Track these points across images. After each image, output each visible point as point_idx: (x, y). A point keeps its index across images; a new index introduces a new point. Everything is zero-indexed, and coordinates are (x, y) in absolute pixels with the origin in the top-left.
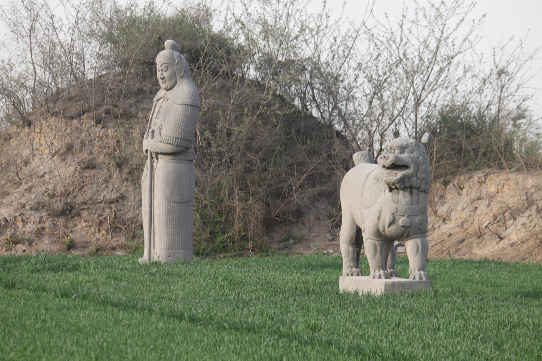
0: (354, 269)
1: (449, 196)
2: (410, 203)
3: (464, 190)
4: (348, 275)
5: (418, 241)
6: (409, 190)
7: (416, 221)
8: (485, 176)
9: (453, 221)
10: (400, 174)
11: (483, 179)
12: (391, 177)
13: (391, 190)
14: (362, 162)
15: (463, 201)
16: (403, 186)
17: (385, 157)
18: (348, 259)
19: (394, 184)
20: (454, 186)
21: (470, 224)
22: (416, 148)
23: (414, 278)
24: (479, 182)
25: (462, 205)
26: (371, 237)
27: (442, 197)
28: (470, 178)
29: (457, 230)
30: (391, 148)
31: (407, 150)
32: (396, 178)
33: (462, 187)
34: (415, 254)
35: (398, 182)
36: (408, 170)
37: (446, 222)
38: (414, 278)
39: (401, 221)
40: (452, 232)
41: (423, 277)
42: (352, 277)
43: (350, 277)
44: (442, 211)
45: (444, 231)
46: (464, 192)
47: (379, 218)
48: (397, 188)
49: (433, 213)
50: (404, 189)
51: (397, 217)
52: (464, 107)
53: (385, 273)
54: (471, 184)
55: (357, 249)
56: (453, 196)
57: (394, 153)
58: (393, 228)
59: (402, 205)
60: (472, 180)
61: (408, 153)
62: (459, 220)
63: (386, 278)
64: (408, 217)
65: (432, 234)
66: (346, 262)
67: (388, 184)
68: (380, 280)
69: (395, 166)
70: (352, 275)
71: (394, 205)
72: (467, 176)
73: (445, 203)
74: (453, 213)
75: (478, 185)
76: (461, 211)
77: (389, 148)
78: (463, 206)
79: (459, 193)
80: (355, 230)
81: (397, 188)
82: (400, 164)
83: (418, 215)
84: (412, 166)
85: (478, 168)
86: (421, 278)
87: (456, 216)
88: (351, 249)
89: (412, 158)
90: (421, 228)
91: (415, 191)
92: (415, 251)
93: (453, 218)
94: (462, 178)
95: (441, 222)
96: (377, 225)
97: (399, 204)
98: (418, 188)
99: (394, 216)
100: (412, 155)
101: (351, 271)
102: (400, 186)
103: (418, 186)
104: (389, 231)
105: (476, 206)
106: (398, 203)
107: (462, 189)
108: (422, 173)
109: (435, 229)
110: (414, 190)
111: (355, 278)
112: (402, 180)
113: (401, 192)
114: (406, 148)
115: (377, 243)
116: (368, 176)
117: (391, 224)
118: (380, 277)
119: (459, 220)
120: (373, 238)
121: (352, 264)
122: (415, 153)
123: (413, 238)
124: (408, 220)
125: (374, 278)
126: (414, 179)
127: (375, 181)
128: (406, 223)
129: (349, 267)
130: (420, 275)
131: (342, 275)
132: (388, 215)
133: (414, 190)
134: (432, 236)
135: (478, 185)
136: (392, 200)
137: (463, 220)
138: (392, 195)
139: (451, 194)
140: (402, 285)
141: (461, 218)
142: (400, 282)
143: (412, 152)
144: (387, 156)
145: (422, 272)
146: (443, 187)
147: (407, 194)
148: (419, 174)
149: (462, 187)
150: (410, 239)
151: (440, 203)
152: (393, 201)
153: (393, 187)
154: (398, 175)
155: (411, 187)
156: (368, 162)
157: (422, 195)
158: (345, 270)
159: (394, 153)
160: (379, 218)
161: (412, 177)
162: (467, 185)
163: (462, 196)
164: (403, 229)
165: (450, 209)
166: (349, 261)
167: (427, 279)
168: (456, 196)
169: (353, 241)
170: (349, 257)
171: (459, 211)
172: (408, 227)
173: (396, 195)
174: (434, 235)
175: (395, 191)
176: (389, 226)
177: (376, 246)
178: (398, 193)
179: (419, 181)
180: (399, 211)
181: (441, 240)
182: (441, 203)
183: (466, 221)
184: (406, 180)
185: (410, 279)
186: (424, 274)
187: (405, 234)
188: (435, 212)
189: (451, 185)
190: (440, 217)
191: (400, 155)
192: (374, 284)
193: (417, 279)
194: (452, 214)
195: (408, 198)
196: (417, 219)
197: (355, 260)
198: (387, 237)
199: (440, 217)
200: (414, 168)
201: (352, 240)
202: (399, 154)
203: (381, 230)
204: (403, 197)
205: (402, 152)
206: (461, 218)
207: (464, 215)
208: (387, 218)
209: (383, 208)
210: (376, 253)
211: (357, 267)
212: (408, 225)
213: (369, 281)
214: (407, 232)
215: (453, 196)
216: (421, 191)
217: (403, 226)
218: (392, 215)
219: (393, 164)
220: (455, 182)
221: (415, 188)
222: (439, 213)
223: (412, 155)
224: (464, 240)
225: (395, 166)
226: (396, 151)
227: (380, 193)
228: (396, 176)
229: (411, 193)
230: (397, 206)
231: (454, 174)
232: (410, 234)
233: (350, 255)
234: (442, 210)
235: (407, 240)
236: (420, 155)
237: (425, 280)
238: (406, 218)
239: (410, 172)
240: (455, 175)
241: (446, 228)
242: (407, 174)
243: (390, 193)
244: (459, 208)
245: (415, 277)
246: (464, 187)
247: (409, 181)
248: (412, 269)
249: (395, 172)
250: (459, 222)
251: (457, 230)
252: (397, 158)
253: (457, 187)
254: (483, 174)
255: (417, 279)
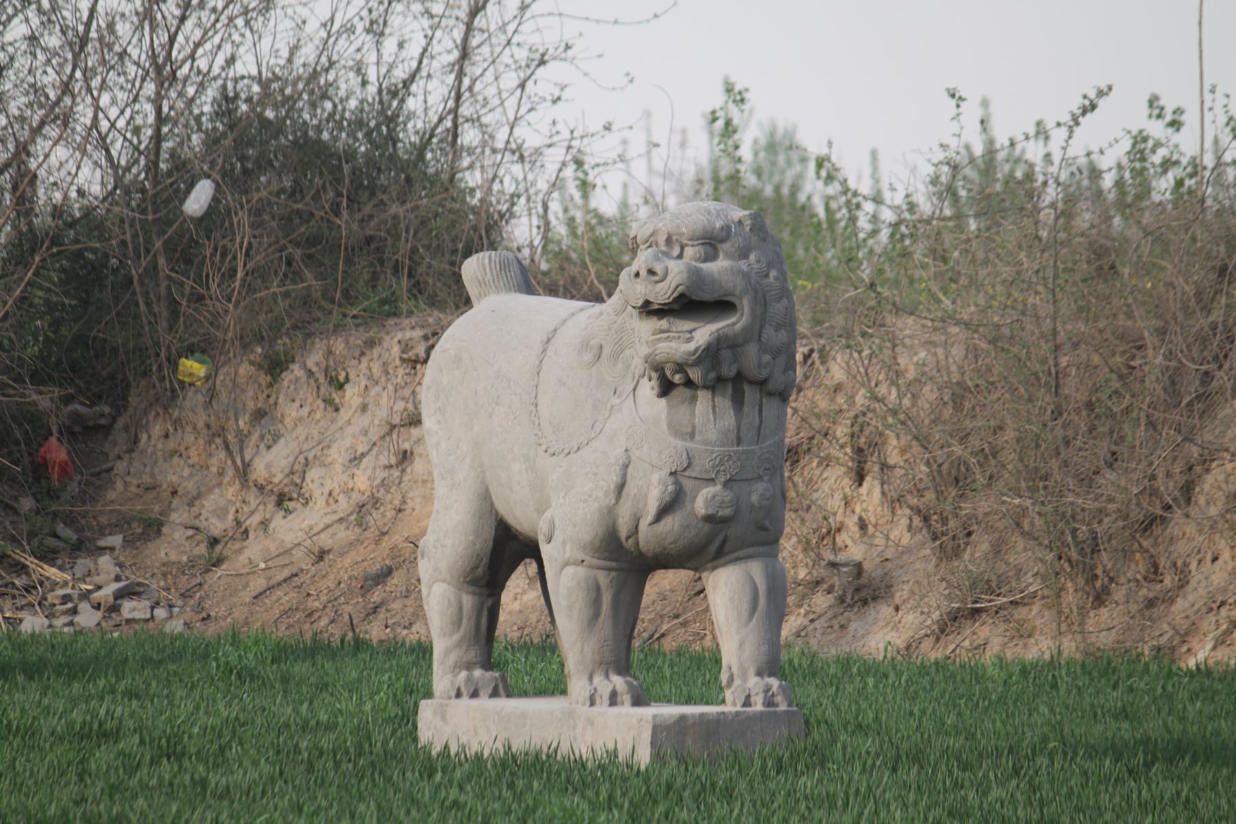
0: (478, 673)
1: (291, 412)
2: (733, 436)
3: (350, 390)
4: (459, 695)
5: (756, 568)
6: (730, 391)
7: (754, 498)
8: (426, 338)
9: (319, 502)
10: (703, 333)
11: (421, 350)
12: (673, 344)
13: (666, 388)
14: (498, 290)
15: (349, 430)
16: (712, 375)
17: (651, 272)
18: (456, 637)
19: (680, 368)
20: (310, 373)
21: (390, 514)
22: (754, 240)
23: (747, 703)
24: (403, 360)
25: (348, 442)
26: (580, 555)
27: (260, 415)
28: (371, 344)
29: (343, 534)
30: (669, 242)
31: (727, 246)
32: (691, 346)
33: (342, 378)
34: (745, 614)
35: (697, 363)
36: (733, 320)
37: (291, 505)
38: (747, 703)
39: (703, 501)
40: (325, 540)
41: (779, 699)
42: (475, 702)
43: (465, 701)
44: (268, 466)
45: (289, 539)
46: (352, 395)
47: (621, 487)
48: (689, 383)
49: (230, 472)
50: (714, 386)
51: (688, 484)
52: (316, 83)
53: (630, 685)
54: (376, 369)
55: (490, 602)
56: (306, 410)
57: (680, 256)
58: (671, 523)
59: (706, 443)
60: (376, 352)
61: (729, 256)
62: (341, 498)
63: (638, 702)
64: (726, 484)
65: (240, 551)
66: (445, 646)
67: (659, 369)
68: (615, 710)
69: (688, 305)
70: (475, 695)
71: (680, 444)
72: (358, 337)
73: (277, 437)
74: (314, 474)
75: (401, 371)
76: (346, 468)
77: (662, 239)
78: (353, 448)
79: (328, 402)
80: (489, 533)
81: (689, 383)
82: (707, 297)
83: (760, 478)
84: (746, 304)
85: (389, 310)
86: (769, 703)
87: (329, 486)
88: (468, 601)
89: (746, 276)
90: (767, 523)
91: (750, 394)
92: (745, 607)
93: (317, 494)
94: (339, 345)
95: (271, 506)
96: (610, 513)
97: (697, 437)
98: (762, 384)
99: (677, 483)
100: (743, 265)
101: (469, 680)
102: (704, 377)
103: (765, 373)
104: (649, 536)
105: (407, 446)
106: (692, 435)
107: (341, 386)
108: (777, 329)
109: (246, 532)
110: (746, 387)
111: (485, 703)
112: (711, 354)
113: (703, 396)
114: (723, 241)
115: (603, 578)
116: (549, 340)
117: (664, 511)
118: (614, 700)
119: (341, 498)
120: (588, 559)
121: (472, 655)
122: (753, 257)
123: (738, 559)
124: (728, 496)
125: (592, 704)
126: (752, 349)
127: (588, 357)
128: (722, 505)
129: (457, 667)
130: (766, 691)
131: (429, 694)
132: (655, 478)
133: (746, 387)
134: (243, 559)
135: (401, 371)
136: (670, 425)
137: (356, 497)
138: (669, 406)
139: (296, 405)
140: (712, 728)
141: (348, 492)
142: (702, 715)
143: (744, 254)
144: (658, 268)
145: (774, 683)
146: (264, 379)
147: (724, 402)
148: (769, 332)
149: (342, 378)
150: (725, 565)
151: (255, 437)
152: (675, 430)
153: (677, 378)
154: (697, 334)
155: (739, 380)
156: (520, 290)
157: (771, 407)
158: (441, 681)
159: (680, 256)
160: (621, 487)
161: (746, 342)
162: (358, 375)
163: (344, 414)
164: (707, 528)
165: (301, 459)
166: (459, 644)
167: (790, 705)
168: (318, 415)
169: (480, 571)
170: (462, 630)
171: (338, 468)
172: (725, 521)
173: (684, 409)
174: (247, 553)
175: (680, 393)
176: (659, 517)
177: (598, 589)
178: (694, 399)
179: (767, 358)
180: (696, 462)
181: (286, 573)
182: (262, 438)
183: (376, 502)
184: (726, 354)
185: (731, 705)
186: (781, 686)
187: (703, 551)
188: (244, 472)
189: (296, 370)
190: (261, 488)
191: (703, 266)
192: (600, 723)
193: (758, 706)
194: (309, 476)
195: (728, 419)
196: (757, 493)
197: (483, 640)
198: (641, 555)
199: (261, 488)
200: (753, 311)
201: (475, 568)
202: (698, 260)
203: (623, 534)
204: (710, 416)
205: (711, 257)
206: (348, 492)
207: (362, 481)
208: (651, 489)
209: (635, 454)
210: (596, 615)
211: (487, 665)
212: (727, 512)
213: (570, 714)
214: (721, 537)
215: (306, 410)
216: (770, 394)
217: (709, 519)
218: (670, 480)
219: (682, 295)
220: (314, 359)
221: (752, 383)
222: (259, 470)
223: (743, 265)
224: (389, 572)
225: (688, 305)
226: (689, 251)
227: (615, 401)
228: (689, 340)
229: (738, 401)
230: (690, 445)
231: (306, 329)
232: (728, 546)
233: (465, 621)
234: (272, 462)
235: (714, 568)
236: (770, 265)
237: (783, 707)
238: (719, 487)
239: (738, 326)
240: (309, 335)
241: (291, 529)
242: (730, 332)
243: (663, 401)
244: (338, 454)
245: (749, 696)
246: (347, 379)
247: (735, 359)
248: (735, 670)
249: (686, 325)
250: (344, 505)
251: (343, 534)
252: (696, 277)
253: (322, 379)
254: (418, 333)
255: (758, 706)
